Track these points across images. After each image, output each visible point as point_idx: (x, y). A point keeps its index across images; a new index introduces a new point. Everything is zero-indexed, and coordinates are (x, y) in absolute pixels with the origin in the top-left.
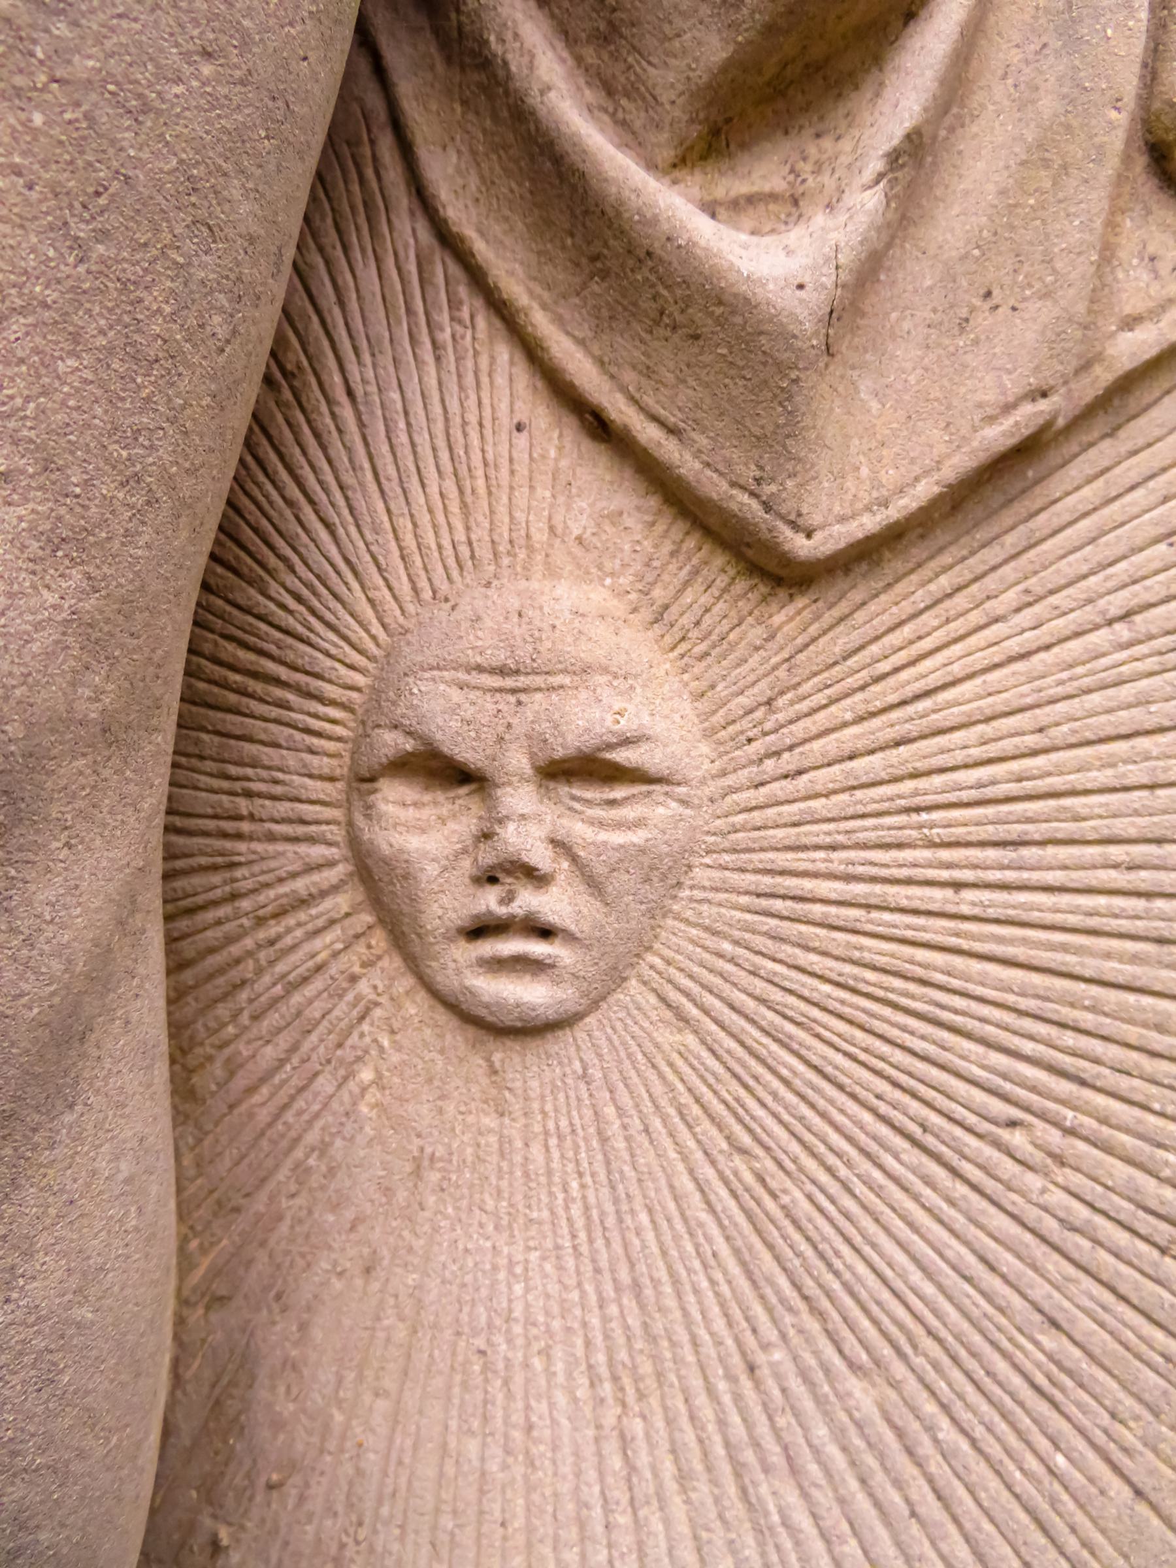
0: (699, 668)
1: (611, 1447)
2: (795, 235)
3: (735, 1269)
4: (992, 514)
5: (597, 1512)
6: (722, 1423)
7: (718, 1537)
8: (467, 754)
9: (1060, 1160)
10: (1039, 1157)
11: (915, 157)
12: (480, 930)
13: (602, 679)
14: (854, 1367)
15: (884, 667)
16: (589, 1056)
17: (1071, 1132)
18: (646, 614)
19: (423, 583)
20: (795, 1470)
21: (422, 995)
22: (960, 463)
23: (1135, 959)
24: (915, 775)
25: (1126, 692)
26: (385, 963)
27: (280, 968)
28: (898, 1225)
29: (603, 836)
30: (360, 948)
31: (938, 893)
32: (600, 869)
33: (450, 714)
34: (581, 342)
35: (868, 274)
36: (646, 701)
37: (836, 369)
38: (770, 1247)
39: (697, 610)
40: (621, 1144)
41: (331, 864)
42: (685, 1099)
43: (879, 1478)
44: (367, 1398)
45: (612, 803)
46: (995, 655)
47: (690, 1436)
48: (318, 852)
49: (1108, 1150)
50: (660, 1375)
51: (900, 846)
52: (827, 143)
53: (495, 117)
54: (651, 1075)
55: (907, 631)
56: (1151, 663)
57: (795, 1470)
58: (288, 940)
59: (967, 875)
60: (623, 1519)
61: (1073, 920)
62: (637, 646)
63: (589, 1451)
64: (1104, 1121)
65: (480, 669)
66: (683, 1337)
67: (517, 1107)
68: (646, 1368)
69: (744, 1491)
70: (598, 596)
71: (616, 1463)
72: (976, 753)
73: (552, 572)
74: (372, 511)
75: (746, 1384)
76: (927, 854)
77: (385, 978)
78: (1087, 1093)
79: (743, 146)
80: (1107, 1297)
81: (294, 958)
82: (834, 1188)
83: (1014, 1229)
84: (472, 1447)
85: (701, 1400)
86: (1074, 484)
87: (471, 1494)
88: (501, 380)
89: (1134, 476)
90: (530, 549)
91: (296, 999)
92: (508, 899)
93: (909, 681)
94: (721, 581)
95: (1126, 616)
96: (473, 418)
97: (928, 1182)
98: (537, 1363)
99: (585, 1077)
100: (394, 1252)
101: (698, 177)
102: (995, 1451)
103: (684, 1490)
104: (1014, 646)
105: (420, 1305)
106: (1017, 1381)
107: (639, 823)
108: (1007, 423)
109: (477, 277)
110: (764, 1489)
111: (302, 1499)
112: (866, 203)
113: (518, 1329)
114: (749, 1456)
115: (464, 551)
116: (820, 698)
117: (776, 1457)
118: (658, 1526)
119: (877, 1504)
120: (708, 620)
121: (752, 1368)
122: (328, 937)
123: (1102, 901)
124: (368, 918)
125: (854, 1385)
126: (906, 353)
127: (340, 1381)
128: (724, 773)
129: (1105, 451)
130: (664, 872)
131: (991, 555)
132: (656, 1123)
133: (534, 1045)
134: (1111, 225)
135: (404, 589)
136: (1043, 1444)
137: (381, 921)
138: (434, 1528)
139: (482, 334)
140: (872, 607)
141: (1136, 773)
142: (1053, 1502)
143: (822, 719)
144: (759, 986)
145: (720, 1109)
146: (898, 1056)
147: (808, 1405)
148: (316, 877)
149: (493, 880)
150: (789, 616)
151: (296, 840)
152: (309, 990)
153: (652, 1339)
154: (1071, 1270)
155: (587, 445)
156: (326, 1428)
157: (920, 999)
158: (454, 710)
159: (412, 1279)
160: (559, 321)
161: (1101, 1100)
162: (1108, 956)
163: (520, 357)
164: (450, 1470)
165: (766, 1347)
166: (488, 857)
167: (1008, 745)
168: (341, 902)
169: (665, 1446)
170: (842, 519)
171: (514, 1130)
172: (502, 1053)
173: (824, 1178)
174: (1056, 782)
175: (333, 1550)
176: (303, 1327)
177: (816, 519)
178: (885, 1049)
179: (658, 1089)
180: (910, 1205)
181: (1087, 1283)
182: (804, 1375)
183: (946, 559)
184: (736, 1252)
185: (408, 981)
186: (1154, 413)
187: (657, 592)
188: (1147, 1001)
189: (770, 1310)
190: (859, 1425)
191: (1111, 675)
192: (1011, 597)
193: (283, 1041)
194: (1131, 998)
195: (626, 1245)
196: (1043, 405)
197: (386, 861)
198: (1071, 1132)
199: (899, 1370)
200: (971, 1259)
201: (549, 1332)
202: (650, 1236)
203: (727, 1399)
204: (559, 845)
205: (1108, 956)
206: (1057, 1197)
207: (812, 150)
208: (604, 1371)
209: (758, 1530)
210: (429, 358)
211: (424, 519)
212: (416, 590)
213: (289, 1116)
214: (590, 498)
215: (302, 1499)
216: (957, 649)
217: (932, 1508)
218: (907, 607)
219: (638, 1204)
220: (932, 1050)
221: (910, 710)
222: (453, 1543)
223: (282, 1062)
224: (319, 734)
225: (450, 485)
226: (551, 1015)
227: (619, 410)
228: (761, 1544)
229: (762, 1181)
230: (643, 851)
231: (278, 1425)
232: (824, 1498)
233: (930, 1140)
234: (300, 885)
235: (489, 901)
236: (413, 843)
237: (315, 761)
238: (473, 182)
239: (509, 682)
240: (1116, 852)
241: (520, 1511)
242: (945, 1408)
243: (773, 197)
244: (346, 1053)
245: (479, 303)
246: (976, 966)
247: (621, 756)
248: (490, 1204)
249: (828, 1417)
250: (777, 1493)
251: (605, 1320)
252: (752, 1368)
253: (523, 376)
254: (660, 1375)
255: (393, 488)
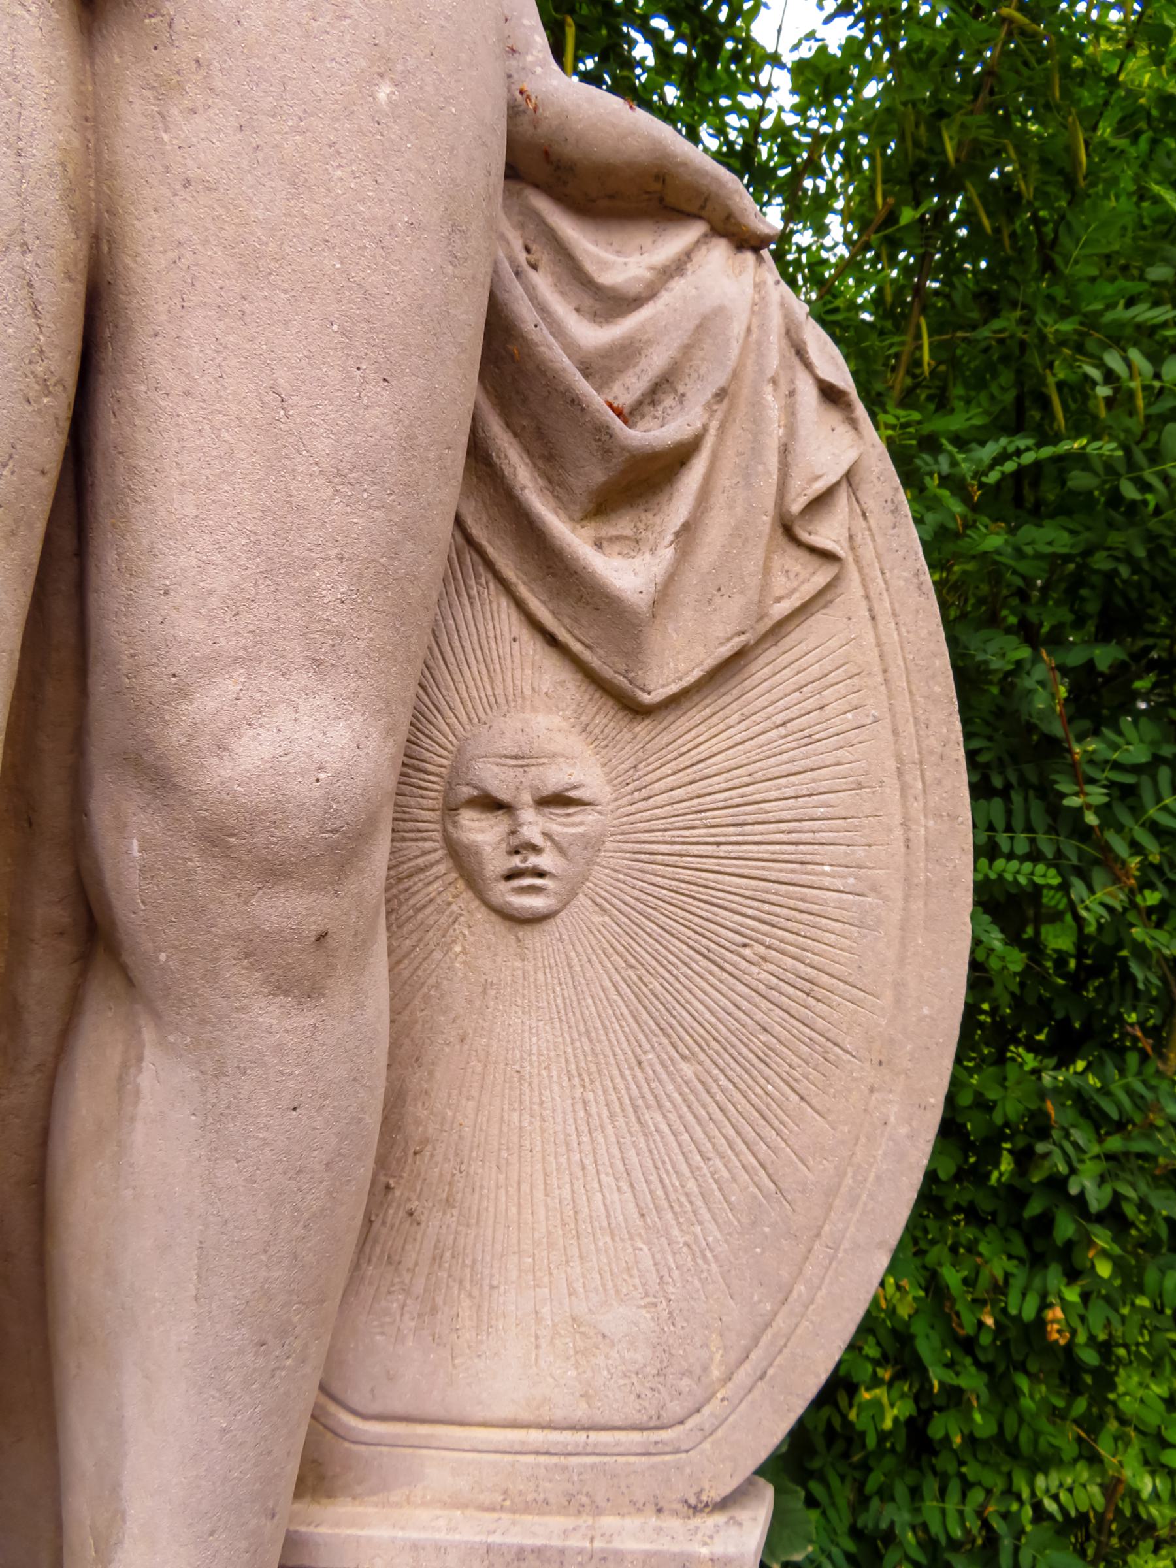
0: (603, 752)
1: (579, 1107)
2: (637, 562)
3: (631, 1020)
4: (728, 680)
5: (574, 1137)
6: (628, 1089)
7: (628, 1140)
8: (503, 795)
9: (765, 959)
10: (756, 959)
11: (687, 533)
12: (511, 876)
13: (562, 760)
14: (683, 1057)
15: (684, 749)
16: (563, 931)
17: (769, 947)
18: (578, 728)
19: (473, 715)
20: (660, 1106)
21: (483, 909)
22: (710, 662)
23: (792, 871)
24: (698, 797)
25: (785, 757)
26: (464, 895)
27: (411, 902)
28: (699, 993)
29: (566, 830)
30: (452, 889)
31: (710, 848)
32: (565, 845)
33: (496, 778)
34: (543, 602)
35: (671, 578)
36: (582, 770)
37: (657, 621)
38: (645, 1008)
39: (602, 726)
40: (578, 969)
41: (435, 850)
42: (606, 945)
43: (696, 1105)
44: (464, 1101)
45: (569, 815)
46: (730, 743)
47: (614, 1097)
48: (428, 845)
49: (784, 953)
50: (599, 1071)
51: (693, 828)
52: (650, 515)
53: (496, 490)
54: (590, 936)
55: (693, 733)
56: (794, 744)
57: (660, 1106)
58: (415, 888)
59: (722, 839)
60: (586, 1139)
61: (766, 856)
62: (575, 743)
63: (569, 1109)
64: (782, 941)
65: (506, 757)
66: (610, 1053)
67: (531, 956)
68: (593, 1069)
69: (638, 1118)
70: (556, 721)
71: (582, 1113)
72: (724, 786)
73: (534, 709)
74: (444, 680)
75: (637, 1070)
76: (704, 831)
77: (465, 901)
78: (775, 930)
79: (613, 510)
80: (786, 1016)
81: (418, 897)
82: (672, 979)
83: (747, 991)
84: (515, 1116)
85: (618, 1080)
86: (760, 669)
87: (515, 1139)
88: (504, 616)
89: (785, 663)
90: (523, 698)
91: (420, 916)
92: (525, 860)
93: (695, 755)
94: (612, 713)
95: (783, 724)
96: (491, 634)
97: (711, 973)
98: (544, 1073)
99: (561, 939)
100: (475, 1031)
101: (593, 524)
102: (743, 1086)
103: (612, 1122)
104: (738, 738)
105: (488, 1054)
106: (751, 1056)
107: (581, 823)
108: (729, 645)
109: (489, 565)
110: (647, 1116)
111: (432, 1156)
112: (667, 554)
113: (534, 1058)
114: (640, 1102)
115: (492, 699)
116: (657, 764)
117: (652, 1102)
118: (601, 1139)
119: (695, 1116)
120: (606, 731)
121: (640, 1063)
122: (436, 885)
123: (778, 847)
124: (455, 875)
125: (684, 1066)
126: (687, 613)
127: (450, 1095)
128: (616, 799)
129: (772, 652)
130: (593, 844)
131: (727, 699)
132: (594, 958)
133: (538, 927)
134: (768, 559)
135: (464, 718)
136: (763, 1082)
137: (462, 876)
138: (499, 1156)
139: (492, 592)
140: (678, 723)
141: (790, 792)
142: (768, 1106)
143: (658, 774)
144: (636, 893)
145: (621, 949)
146: (696, 920)
147: (664, 1076)
148: (428, 857)
149: (517, 852)
150: (643, 728)
151: (417, 840)
152: (427, 911)
153: (595, 1055)
154: (771, 1006)
155: (547, 649)
156: (444, 1118)
157: (704, 894)
158: (496, 776)
159: (484, 1041)
160: (532, 590)
161: (780, 932)
162: (781, 871)
163: (512, 605)
164: (505, 1129)
165: (645, 1052)
166: (514, 842)
167: (737, 782)
168: (441, 868)
169: (603, 1103)
170: (663, 686)
171: (530, 968)
172: (524, 932)
173: (667, 975)
174: (757, 797)
175: (449, 1177)
176: (431, 1073)
177: (651, 687)
178: (691, 917)
179: (594, 942)
180: (704, 984)
181: (777, 1010)
182: (662, 1063)
183: (708, 701)
184: (631, 1012)
185: (477, 903)
186: (793, 635)
187: (583, 718)
188: (797, 889)
189: (646, 1036)
190: (686, 1083)
191: (777, 750)
192: (736, 717)
193: (415, 937)
194: (791, 888)
195: (582, 1014)
196: (743, 638)
197: (466, 847)
198: (769, 947)
199: (702, 1057)
200: (730, 1005)
201: (549, 1058)
202: (593, 1009)
203: (629, 1078)
204: (546, 835)
205: (781, 871)
206: (764, 975)
207: (643, 517)
208: (574, 1073)
209: (645, 1135)
210: (467, 603)
211: (471, 684)
212: (470, 719)
213: (420, 973)
214: (548, 675)
215: (432, 1156)
216: (714, 741)
217: (718, 1115)
218: (693, 723)
219: (587, 995)
220: (710, 916)
221: (695, 768)
222: (508, 1163)
223: (414, 947)
224: (426, 789)
225: (483, 668)
226: (545, 911)
227: (563, 635)
228: (647, 1141)
229: (640, 979)
230: (583, 835)
231: (418, 1122)
232: (673, 1116)
233: (711, 955)
234: (420, 861)
235: (516, 862)
236: (479, 838)
237: (424, 802)
238: (485, 519)
239: (520, 762)
240: (783, 826)
241: (539, 1143)
242: (722, 1071)
243: (627, 538)
244: (448, 939)
245: (490, 576)
246: (727, 878)
247: (573, 794)
248: (520, 1002)
249: (673, 1080)
250: (653, 1118)
251: (574, 1049)
252: (640, 1063)
253: (515, 615)
254: (599, 1071)
255: (454, 668)
